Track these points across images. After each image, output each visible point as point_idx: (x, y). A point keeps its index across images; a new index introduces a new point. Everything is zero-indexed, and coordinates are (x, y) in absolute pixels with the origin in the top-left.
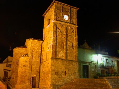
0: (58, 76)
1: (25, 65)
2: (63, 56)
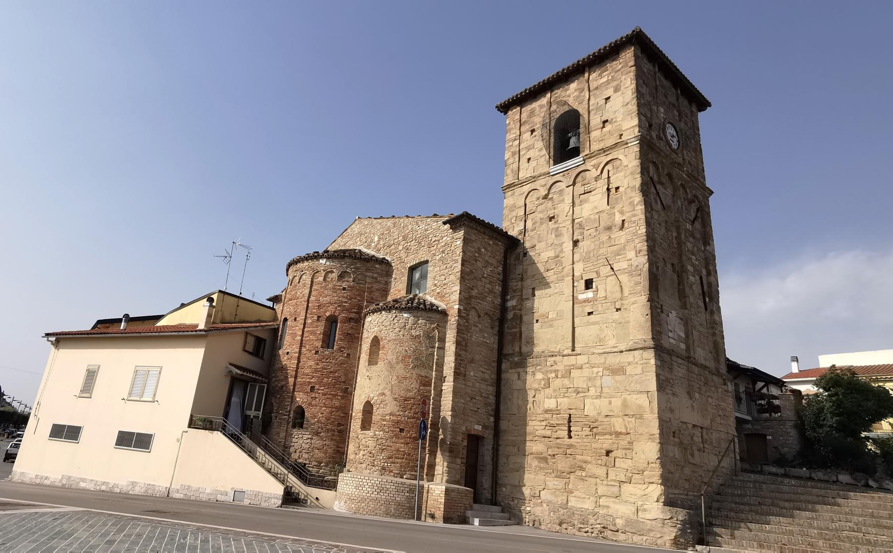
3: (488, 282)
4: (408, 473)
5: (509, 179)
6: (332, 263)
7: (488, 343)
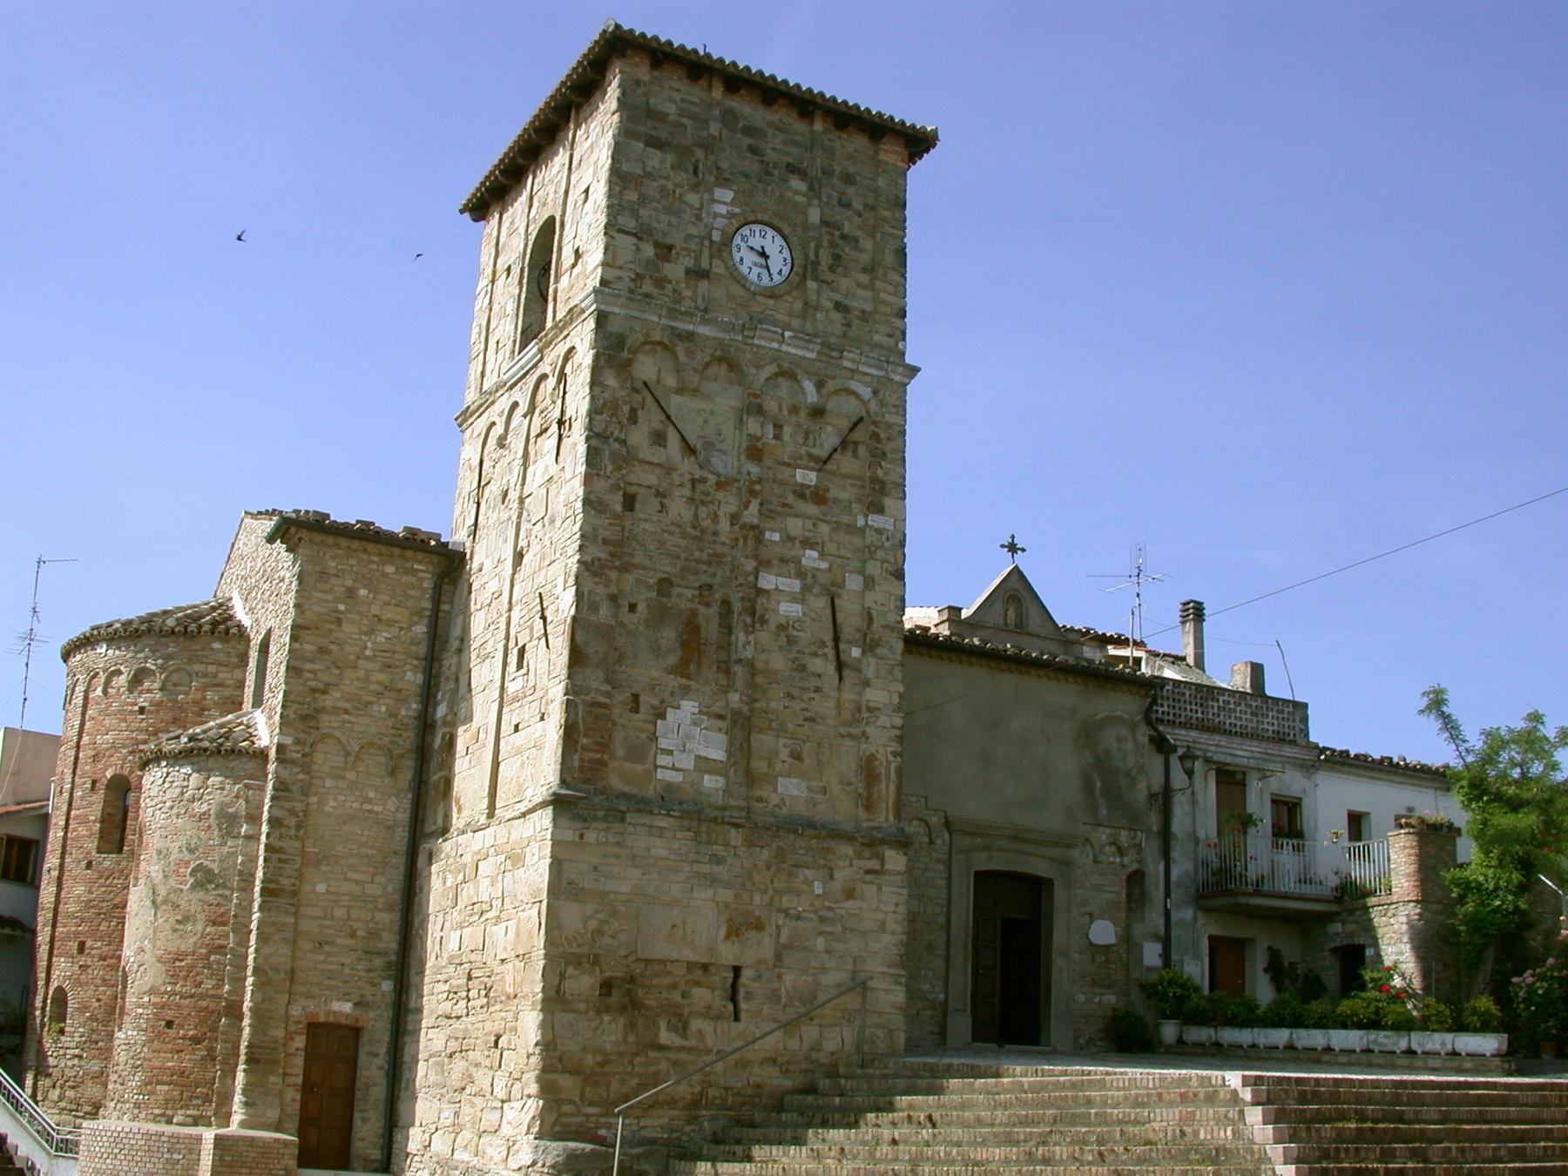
0: (632, 1026)
1: (215, 867)
2: (704, 765)
3: (377, 666)
4: (179, 1112)
5: (471, 397)
6: (117, 652)
7: (377, 813)
